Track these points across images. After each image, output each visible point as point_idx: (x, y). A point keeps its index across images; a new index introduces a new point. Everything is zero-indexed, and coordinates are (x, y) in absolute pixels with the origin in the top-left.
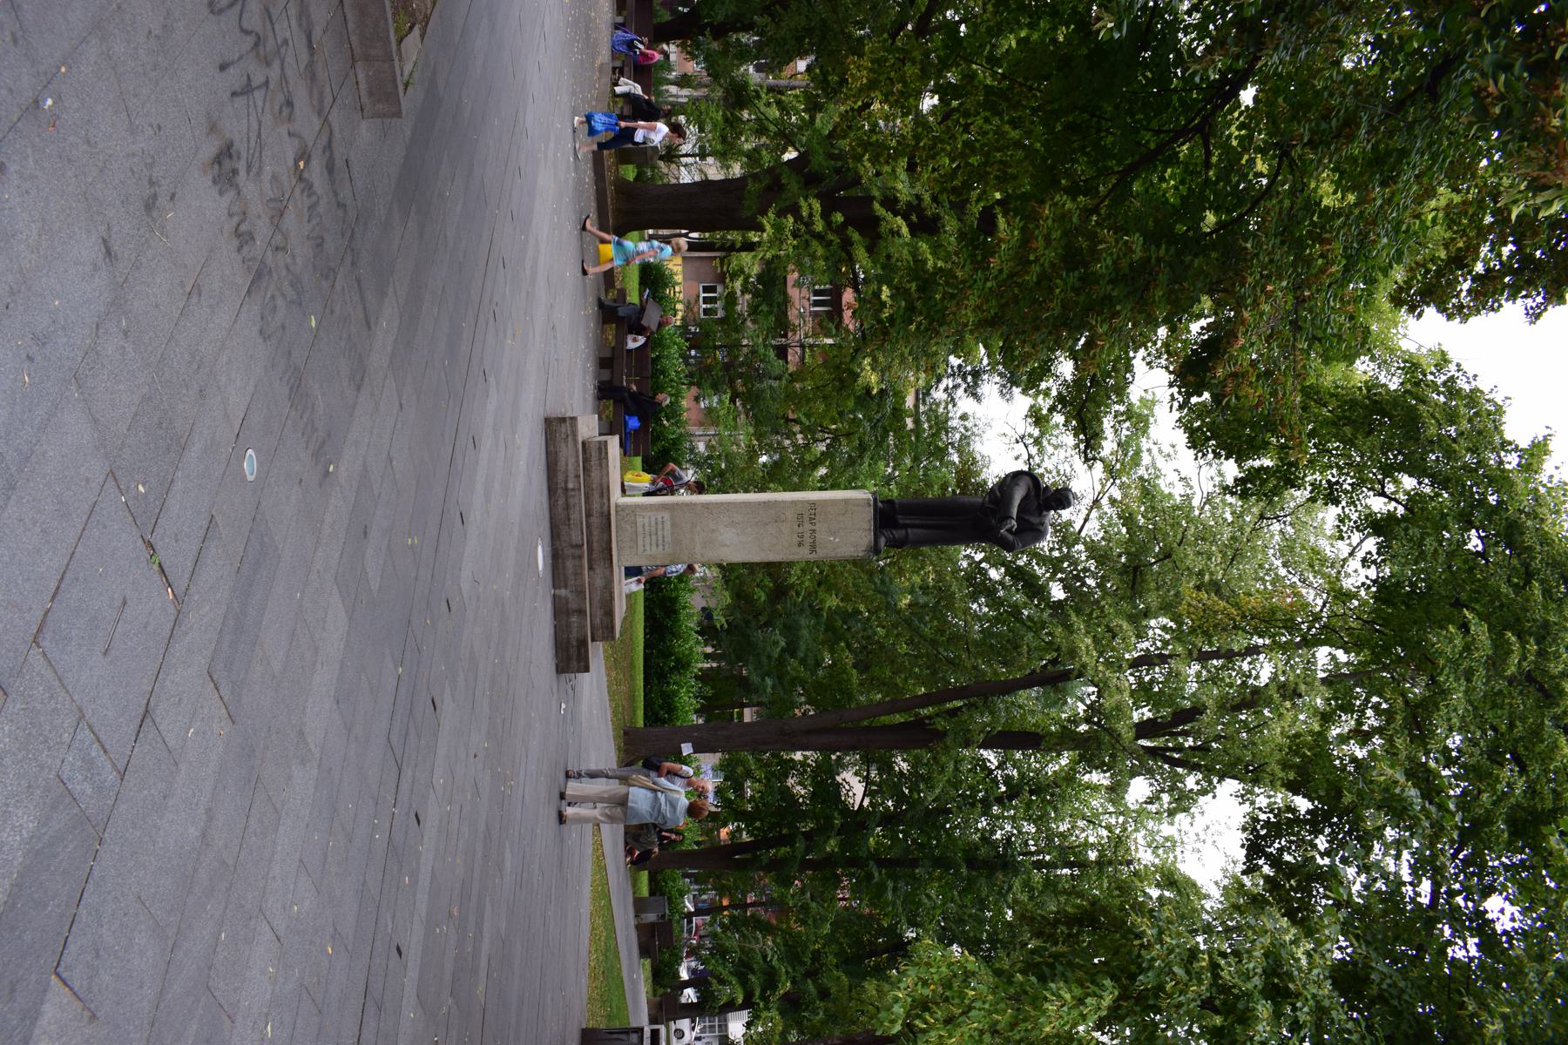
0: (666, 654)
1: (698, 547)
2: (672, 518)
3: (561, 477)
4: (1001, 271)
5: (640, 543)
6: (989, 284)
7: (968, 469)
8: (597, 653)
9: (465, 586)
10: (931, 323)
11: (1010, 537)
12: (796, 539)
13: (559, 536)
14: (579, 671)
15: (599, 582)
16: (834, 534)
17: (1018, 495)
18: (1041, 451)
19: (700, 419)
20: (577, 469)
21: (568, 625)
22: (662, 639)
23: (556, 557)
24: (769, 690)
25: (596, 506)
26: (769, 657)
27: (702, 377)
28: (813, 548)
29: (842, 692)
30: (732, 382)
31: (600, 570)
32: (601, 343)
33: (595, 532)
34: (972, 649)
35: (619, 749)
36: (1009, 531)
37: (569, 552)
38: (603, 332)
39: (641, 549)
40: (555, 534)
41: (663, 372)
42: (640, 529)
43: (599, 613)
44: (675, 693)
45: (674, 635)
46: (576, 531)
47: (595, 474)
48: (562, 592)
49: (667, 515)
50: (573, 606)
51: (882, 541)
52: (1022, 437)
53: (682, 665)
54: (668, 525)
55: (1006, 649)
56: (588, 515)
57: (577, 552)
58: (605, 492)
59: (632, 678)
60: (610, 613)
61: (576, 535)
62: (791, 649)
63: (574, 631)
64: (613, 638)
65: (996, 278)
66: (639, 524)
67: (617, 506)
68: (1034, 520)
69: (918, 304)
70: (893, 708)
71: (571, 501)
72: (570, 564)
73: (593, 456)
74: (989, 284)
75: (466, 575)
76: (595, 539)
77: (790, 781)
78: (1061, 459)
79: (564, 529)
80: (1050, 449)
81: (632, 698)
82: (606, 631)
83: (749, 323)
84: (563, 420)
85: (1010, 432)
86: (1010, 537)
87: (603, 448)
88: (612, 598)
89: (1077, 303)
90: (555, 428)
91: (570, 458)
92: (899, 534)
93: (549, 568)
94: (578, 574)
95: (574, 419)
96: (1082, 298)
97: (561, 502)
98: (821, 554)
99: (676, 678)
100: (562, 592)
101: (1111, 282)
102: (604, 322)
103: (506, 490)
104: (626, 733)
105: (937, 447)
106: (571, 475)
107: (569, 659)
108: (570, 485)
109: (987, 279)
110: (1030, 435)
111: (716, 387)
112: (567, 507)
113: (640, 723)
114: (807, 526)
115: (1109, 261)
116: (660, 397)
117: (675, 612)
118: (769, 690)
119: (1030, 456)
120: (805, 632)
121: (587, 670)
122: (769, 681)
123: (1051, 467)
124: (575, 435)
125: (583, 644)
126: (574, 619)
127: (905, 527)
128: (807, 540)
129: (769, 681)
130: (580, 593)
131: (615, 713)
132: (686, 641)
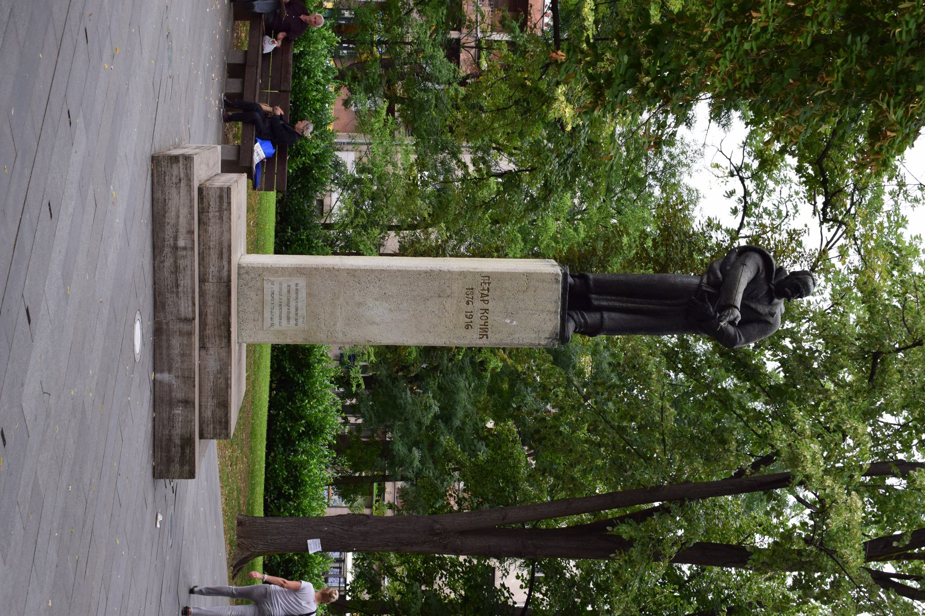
0: (295, 417)
1: (339, 326)
2: (309, 286)
3: (169, 232)
4: (764, 29)
5: (267, 315)
6: (747, 46)
7: (673, 219)
8: (209, 455)
9: (29, 406)
10: (660, 88)
11: (731, 329)
12: (463, 320)
13: (163, 306)
14: (181, 477)
15: (212, 365)
16: (511, 315)
17: (745, 277)
18: (761, 188)
19: (353, 141)
20: (190, 224)
21: (171, 419)
22: (291, 398)
23: (159, 334)
24: (416, 463)
25: (213, 270)
26: (419, 423)
27: (353, 77)
28: (484, 332)
29: (507, 480)
30: (390, 84)
31: (214, 350)
32: (231, 43)
33: (211, 302)
34: (669, 441)
35: (231, 543)
36: (732, 323)
37: (176, 326)
38: (233, 30)
39: (267, 323)
40: (159, 304)
41: (307, 72)
42: (268, 298)
43: (210, 403)
44: (304, 465)
45: (305, 393)
46: (186, 301)
47: (213, 229)
48: (165, 377)
49: (302, 282)
50: (178, 395)
51: (571, 326)
52: (739, 170)
53: (314, 431)
54: (303, 294)
55: (712, 443)
56: (203, 280)
57: (185, 327)
58: (225, 252)
59: (252, 450)
60: (224, 405)
61: (185, 305)
62: (446, 416)
63: (178, 425)
64: (227, 436)
65: (757, 37)
66: (267, 292)
67: (240, 267)
68: (763, 309)
69: (645, 62)
70: (567, 508)
71: (181, 262)
72: (176, 342)
73: (212, 204)
74: (747, 46)
75: (31, 388)
76: (210, 310)
77: (438, 582)
78: (798, 219)
79: (170, 299)
80: (771, 184)
81: (250, 474)
82: (218, 427)
83: (415, 15)
84: (175, 159)
85: (725, 163)
86: (731, 329)
87: (225, 194)
88: (228, 386)
89: (862, 80)
90: (165, 168)
91: (182, 208)
92: (592, 318)
93: (149, 347)
94: (186, 355)
95: (188, 159)
96: (870, 74)
97: (169, 263)
98: (493, 339)
99: (305, 445)
100: (165, 377)
101: (912, 51)
102: (227, 119)
103: (98, 251)
104: (240, 523)
105: (635, 176)
106: (183, 230)
107: (170, 460)
108: (181, 243)
109: (744, 39)
110: (747, 167)
111: (369, 90)
112: (176, 270)
113: (259, 512)
114: (478, 304)
115: (912, 25)
116: (300, 125)
117: (309, 366)
118: (416, 463)
119: (747, 193)
120: (463, 396)
121: (191, 475)
122: (416, 453)
123: (771, 208)
124: (189, 179)
125: (188, 443)
126: (178, 411)
127: (600, 309)
128: (477, 322)
129: (416, 453)
130: (188, 379)
131: (227, 500)
132: (320, 402)
